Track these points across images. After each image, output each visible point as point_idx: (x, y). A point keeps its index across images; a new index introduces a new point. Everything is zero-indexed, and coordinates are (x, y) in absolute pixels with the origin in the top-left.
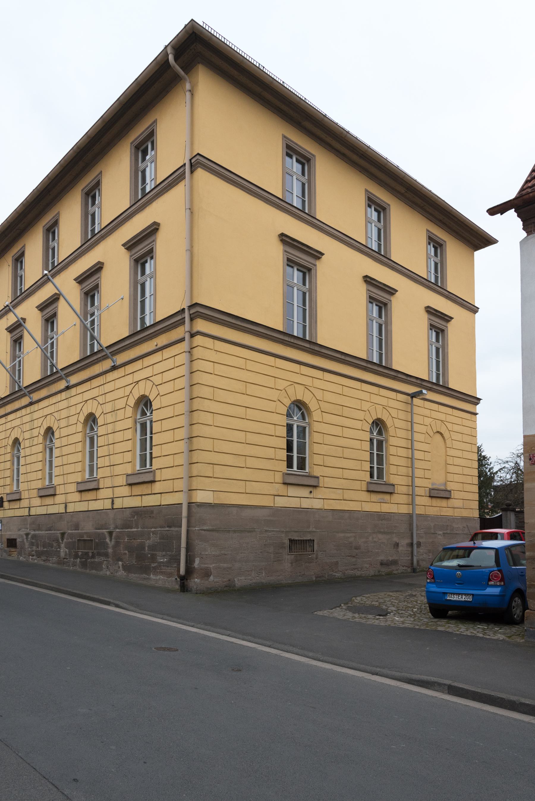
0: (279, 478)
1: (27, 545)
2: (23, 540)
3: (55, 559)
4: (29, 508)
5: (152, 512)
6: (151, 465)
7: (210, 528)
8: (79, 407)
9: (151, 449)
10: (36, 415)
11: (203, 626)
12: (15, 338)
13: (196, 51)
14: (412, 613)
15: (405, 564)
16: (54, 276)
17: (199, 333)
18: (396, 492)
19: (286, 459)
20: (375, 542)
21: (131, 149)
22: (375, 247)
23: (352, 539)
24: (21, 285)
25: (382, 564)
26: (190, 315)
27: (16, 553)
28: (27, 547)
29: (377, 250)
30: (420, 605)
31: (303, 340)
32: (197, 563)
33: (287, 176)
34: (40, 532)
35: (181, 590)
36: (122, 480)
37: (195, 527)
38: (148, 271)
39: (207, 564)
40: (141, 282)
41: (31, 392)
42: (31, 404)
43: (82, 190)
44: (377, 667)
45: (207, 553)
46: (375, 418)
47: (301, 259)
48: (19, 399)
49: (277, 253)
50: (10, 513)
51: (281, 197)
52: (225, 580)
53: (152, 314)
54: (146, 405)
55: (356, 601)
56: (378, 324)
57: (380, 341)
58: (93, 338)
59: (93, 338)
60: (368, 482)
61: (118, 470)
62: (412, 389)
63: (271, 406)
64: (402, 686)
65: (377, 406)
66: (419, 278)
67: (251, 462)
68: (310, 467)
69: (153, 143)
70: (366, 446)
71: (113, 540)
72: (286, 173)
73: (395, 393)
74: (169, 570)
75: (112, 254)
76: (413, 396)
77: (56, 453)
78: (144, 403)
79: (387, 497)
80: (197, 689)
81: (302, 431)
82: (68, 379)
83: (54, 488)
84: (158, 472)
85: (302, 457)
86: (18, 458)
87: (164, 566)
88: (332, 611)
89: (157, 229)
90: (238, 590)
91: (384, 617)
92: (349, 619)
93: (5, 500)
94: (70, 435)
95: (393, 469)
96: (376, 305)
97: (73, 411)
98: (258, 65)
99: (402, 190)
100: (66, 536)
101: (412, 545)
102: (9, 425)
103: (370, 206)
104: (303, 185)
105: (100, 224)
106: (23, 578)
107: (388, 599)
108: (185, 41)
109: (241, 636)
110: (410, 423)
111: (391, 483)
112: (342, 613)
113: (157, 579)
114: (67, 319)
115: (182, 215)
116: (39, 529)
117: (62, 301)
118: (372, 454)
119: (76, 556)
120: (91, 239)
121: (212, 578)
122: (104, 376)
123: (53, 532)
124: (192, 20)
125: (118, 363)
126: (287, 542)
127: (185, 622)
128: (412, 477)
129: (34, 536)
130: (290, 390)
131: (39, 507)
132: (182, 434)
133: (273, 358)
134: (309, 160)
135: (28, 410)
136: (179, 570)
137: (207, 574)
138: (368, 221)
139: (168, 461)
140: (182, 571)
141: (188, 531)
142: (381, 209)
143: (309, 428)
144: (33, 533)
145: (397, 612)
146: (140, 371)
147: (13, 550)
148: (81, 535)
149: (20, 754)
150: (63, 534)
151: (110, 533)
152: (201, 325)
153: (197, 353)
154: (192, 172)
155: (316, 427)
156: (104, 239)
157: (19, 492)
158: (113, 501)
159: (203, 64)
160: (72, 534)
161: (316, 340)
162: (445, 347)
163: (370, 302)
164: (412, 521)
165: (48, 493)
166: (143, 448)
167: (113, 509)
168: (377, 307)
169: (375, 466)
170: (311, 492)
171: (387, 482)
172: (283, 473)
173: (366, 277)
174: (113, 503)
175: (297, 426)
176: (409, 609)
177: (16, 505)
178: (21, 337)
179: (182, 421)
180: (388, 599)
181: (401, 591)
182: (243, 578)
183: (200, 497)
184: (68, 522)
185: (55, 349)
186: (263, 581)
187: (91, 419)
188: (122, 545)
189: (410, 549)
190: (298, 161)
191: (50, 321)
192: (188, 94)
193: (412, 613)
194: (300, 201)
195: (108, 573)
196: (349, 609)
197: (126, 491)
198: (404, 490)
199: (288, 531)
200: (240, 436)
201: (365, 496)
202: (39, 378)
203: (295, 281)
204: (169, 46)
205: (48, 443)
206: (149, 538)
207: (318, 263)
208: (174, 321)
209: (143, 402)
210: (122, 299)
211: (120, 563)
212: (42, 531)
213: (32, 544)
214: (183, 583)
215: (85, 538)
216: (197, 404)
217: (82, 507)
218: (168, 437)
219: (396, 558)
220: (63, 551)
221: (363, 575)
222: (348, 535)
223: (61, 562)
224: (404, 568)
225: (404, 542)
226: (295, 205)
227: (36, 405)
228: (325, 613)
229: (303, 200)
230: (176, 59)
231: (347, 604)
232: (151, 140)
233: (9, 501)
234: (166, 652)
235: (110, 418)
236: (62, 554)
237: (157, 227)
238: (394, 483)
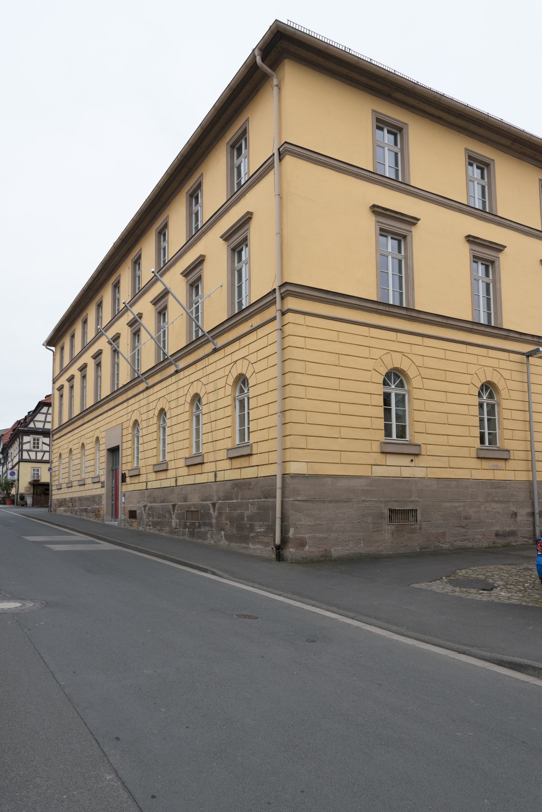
0: (376, 447)
1: (145, 516)
2: (142, 511)
3: (167, 529)
4: (147, 482)
5: (250, 484)
6: (249, 440)
7: (305, 498)
8: (186, 388)
9: (249, 424)
10: (151, 399)
11: (290, 595)
12: (134, 331)
13: (284, 46)
14: (523, 589)
15: (525, 535)
16: (162, 275)
17: (290, 311)
18: (512, 458)
19: (383, 428)
20: (488, 511)
21: (227, 149)
22: (478, 205)
23: (461, 509)
24: (139, 284)
25: (497, 535)
26: (281, 294)
27: (136, 523)
28: (145, 518)
29: (481, 208)
30: (533, 580)
31: (401, 307)
32: (291, 533)
33: (378, 148)
34: (155, 504)
35: (277, 559)
36: (223, 455)
37: (289, 498)
38: (243, 258)
39: (302, 534)
40: (238, 269)
41: (147, 378)
42: (147, 388)
43: (187, 193)
44: (465, 645)
45: (301, 523)
46: (483, 381)
47: (395, 227)
48: (137, 385)
49: (369, 224)
50: (131, 488)
51: (372, 170)
52: (321, 550)
53: (248, 297)
54: (244, 383)
55: (460, 574)
56: (485, 284)
57: (488, 300)
58: (197, 326)
59: (197, 326)
60: (477, 449)
61: (221, 445)
62: (527, 348)
63: (366, 376)
64: (490, 668)
65: (485, 368)
66: (531, 230)
67: (345, 432)
68: (410, 435)
69: (246, 140)
70: (476, 410)
71: (216, 511)
72: (377, 145)
73: (508, 353)
74: (266, 539)
75: (213, 247)
76: (528, 355)
77: (204, 419)
78: (242, 381)
79: (501, 464)
80: (263, 657)
81: (401, 400)
82: (177, 364)
83: (166, 463)
84: (255, 446)
85: (402, 425)
86: (138, 437)
87: (261, 536)
88: (431, 583)
89: (251, 218)
90: (335, 560)
91: (489, 592)
92: (448, 592)
93: (127, 475)
94: (179, 414)
95: (507, 434)
96: (482, 264)
97: (181, 392)
98: (343, 49)
99: (508, 143)
100: (176, 507)
101: (533, 514)
102: (130, 409)
103: (471, 165)
104: (396, 154)
105: (202, 221)
106: (137, 546)
107: (497, 573)
108: (271, 40)
109: (325, 606)
110: (527, 384)
111: (506, 448)
112: (441, 587)
113: (255, 548)
114: (176, 313)
115: (273, 201)
116: (155, 502)
117: (170, 297)
118: (481, 420)
119: (185, 526)
120: (195, 235)
121: (307, 548)
122: (207, 359)
123: (166, 504)
124: (276, 20)
125: (219, 345)
126: (387, 512)
127: (273, 591)
128: (531, 441)
129: (151, 508)
130: (387, 359)
131: (155, 482)
132: (275, 408)
133: (367, 328)
134: (401, 130)
135: (145, 394)
136: (274, 540)
137: (302, 544)
138: (469, 180)
139: (263, 435)
140: (278, 541)
141: (282, 502)
142: (484, 166)
143: (409, 395)
144: (149, 505)
145: (505, 587)
146: (237, 351)
147: (133, 520)
148: (189, 506)
149: (78, 709)
150: (174, 506)
151: (214, 505)
152: (292, 303)
153: (288, 329)
154: (280, 160)
155: (416, 394)
156: (205, 234)
157: (138, 468)
158: (216, 474)
159: (289, 58)
160: (182, 505)
161: (414, 306)
162: (496, 281)
163: (474, 261)
164: (533, 488)
165: (161, 468)
166: (242, 423)
167: (216, 481)
168: (484, 267)
169: (486, 431)
170: (412, 461)
171: (501, 448)
172: (381, 442)
173: (374, 206)
174: (216, 476)
175: (396, 394)
176: (520, 584)
177: (135, 480)
178: (139, 330)
179: (275, 396)
180: (497, 573)
181: (515, 565)
182: (339, 548)
183: (294, 468)
184: (178, 495)
185: (166, 338)
186: (361, 551)
187: (197, 399)
188: (224, 516)
189: (531, 519)
190: (389, 132)
191: (162, 313)
192: (276, 89)
193: (523, 589)
194: (393, 171)
195: (212, 542)
196: (450, 582)
197: (226, 464)
198: (522, 455)
199: (386, 501)
200: (334, 407)
201: (476, 463)
202: (153, 365)
203: (480, 275)
204: (257, 49)
205: (161, 423)
206: (248, 509)
207: (413, 229)
208: (266, 302)
209: (241, 380)
210: (221, 286)
211: (223, 532)
212: (157, 503)
213: (149, 515)
214: (279, 552)
215: (193, 509)
216: (288, 379)
217: (190, 480)
218: (262, 412)
219: (515, 529)
220: (174, 521)
221: (475, 547)
222: (457, 504)
223: (172, 532)
224: (525, 539)
225: (523, 512)
226: (388, 176)
227: (151, 389)
228: (423, 585)
229: (396, 169)
230: (263, 59)
231: (449, 576)
232: (245, 137)
233: (131, 476)
234: (246, 620)
235: (212, 397)
236: (174, 525)
237: (250, 216)
238: (509, 449)
